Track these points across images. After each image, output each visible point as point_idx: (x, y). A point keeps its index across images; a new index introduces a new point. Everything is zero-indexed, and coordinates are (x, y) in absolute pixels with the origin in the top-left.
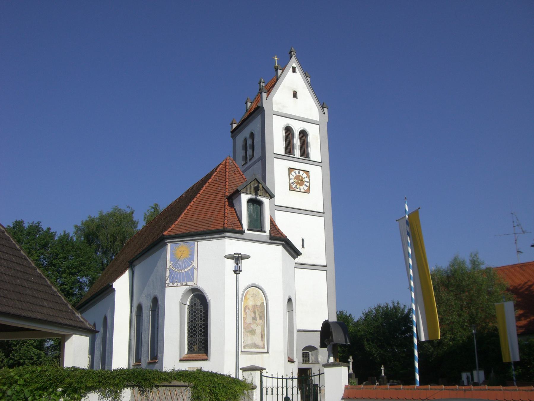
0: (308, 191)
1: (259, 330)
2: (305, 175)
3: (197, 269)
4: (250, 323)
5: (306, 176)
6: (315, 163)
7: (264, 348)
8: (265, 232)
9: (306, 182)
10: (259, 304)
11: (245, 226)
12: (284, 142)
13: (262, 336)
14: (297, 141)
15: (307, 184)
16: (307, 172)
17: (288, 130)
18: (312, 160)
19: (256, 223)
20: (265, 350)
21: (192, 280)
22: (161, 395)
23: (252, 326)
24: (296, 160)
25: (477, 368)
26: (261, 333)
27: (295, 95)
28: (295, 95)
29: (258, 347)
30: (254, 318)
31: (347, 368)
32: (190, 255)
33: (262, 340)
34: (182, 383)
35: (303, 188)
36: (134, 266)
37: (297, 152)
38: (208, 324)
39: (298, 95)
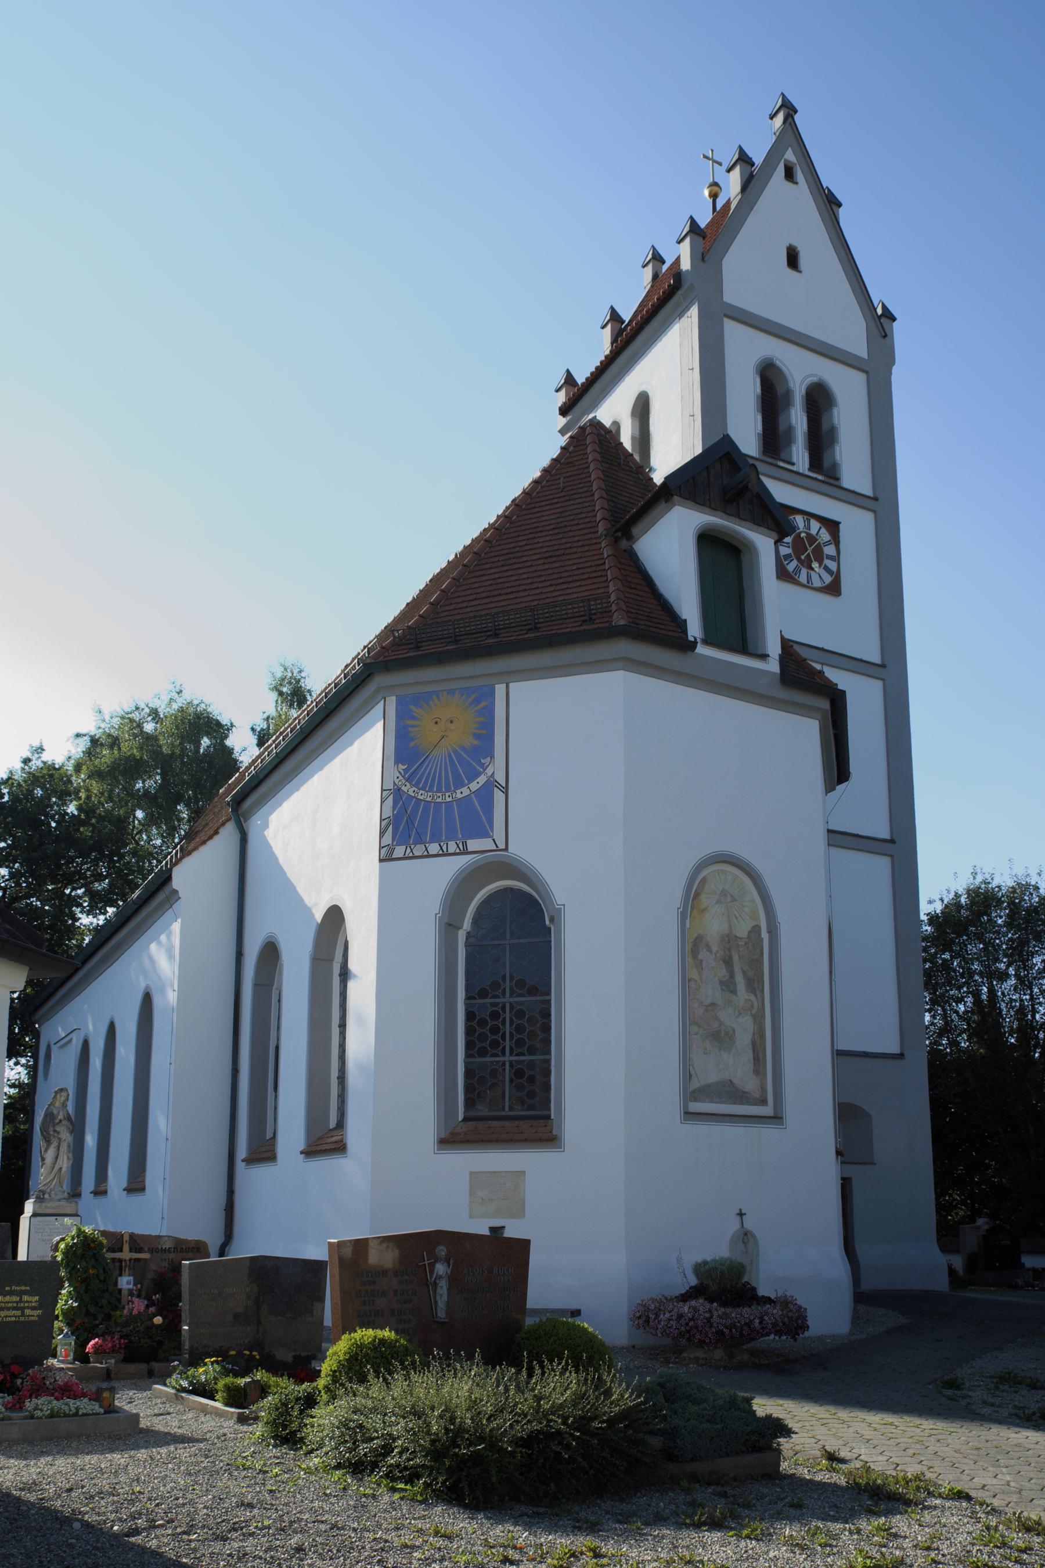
0: (834, 588)
1: (743, 1030)
2: (825, 536)
3: (506, 791)
6: (853, 498)
7: (763, 1102)
8: (764, 657)
9: (829, 557)
10: (742, 930)
12: (759, 418)
13: (758, 1059)
14: (798, 419)
15: (832, 565)
16: (832, 526)
19: (732, 617)
20: (768, 1110)
21: (484, 832)
22: (149, 1412)
23: (722, 1015)
26: (754, 1044)
27: (793, 259)
28: (793, 259)
29: (738, 1096)
30: (728, 985)
32: (476, 736)
35: (819, 576)
37: (800, 455)
39: (803, 260)
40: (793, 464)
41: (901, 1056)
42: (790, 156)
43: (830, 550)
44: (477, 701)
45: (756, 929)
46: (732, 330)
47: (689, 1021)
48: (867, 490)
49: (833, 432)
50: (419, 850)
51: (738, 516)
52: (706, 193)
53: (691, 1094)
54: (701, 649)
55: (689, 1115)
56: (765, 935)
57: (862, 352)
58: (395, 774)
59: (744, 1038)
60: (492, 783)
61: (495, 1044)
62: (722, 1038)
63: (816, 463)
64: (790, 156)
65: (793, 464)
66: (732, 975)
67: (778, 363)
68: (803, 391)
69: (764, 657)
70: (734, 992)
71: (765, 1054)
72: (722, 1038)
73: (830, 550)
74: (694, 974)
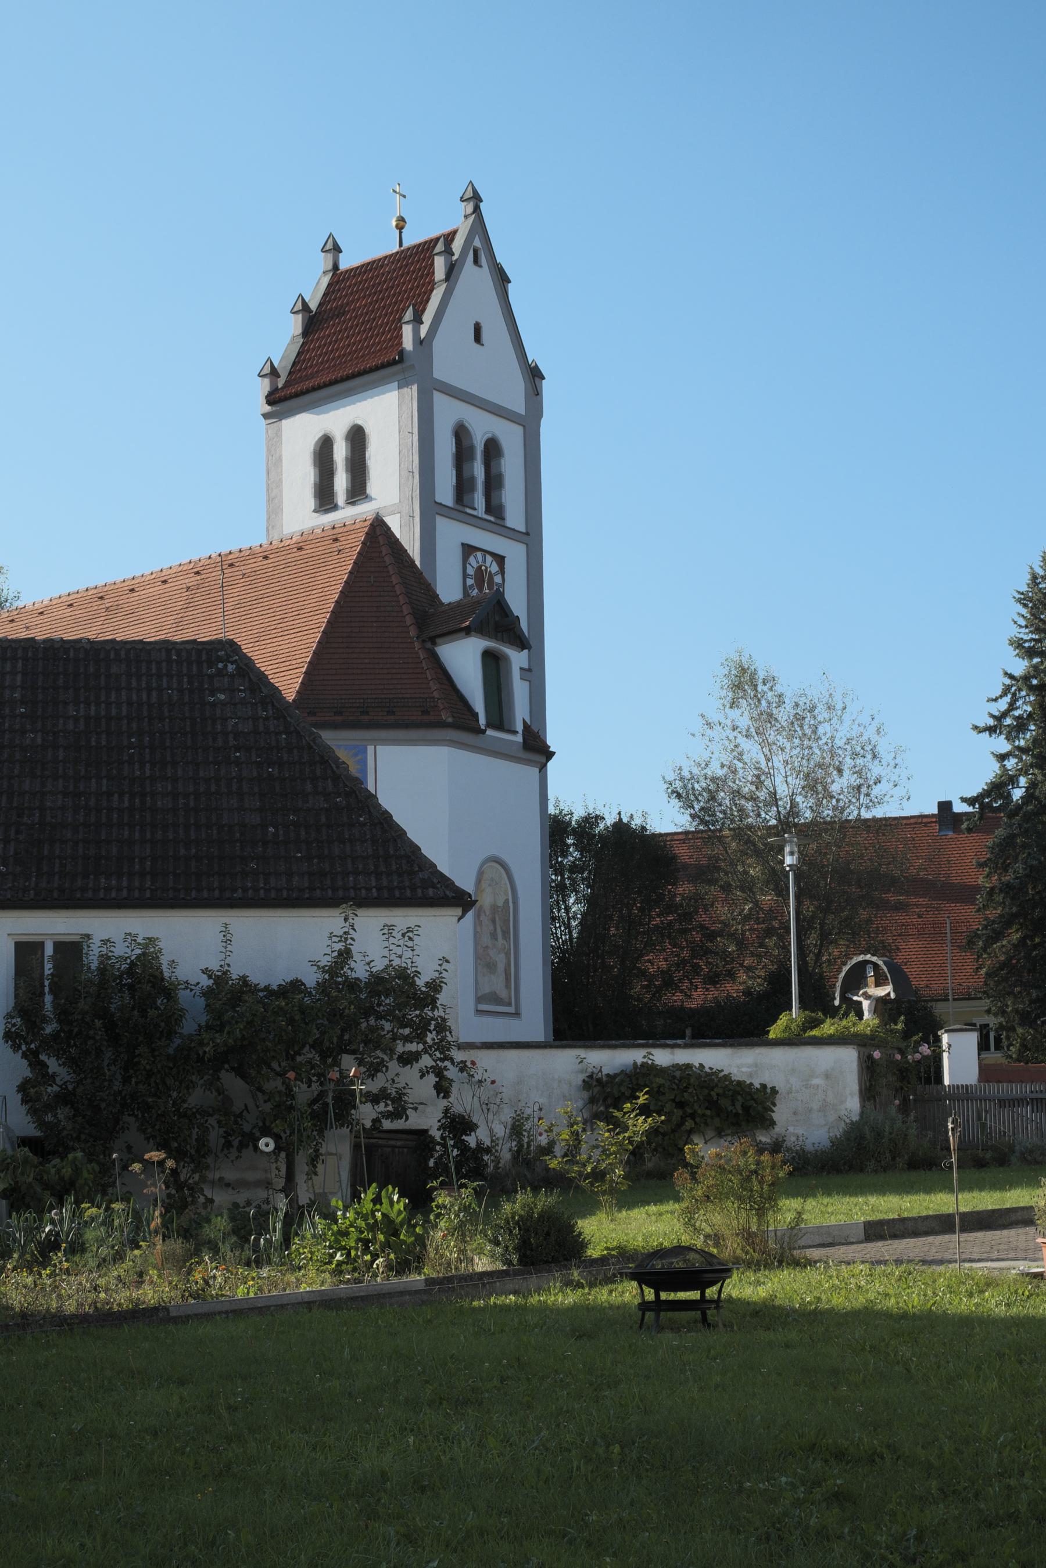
1: (500, 960)
2: (494, 568)
4: (487, 947)
6: (512, 534)
7: (509, 1004)
8: (515, 732)
10: (500, 903)
12: (454, 472)
16: (500, 560)
17: (461, 433)
20: (512, 1010)
24: (475, 522)
25: (49, 950)
30: (494, 936)
31: (541, 1038)
33: (508, 986)
37: (479, 500)
38: (66, 907)
40: (475, 509)
42: (477, 243)
44: (356, 755)
45: (507, 901)
46: (439, 398)
47: (477, 957)
48: (522, 528)
49: (500, 477)
51: (503, 641)
52: (394, 223)
53: (479, 1000)
54: (490, 732)
55: (479, 1012)
56: (511, 904)
57: (522, 411)
59: (501, 966)
62: (491, 967)
63: (489, 510)
64: (477, 243)
65: (475, 509)
66: (495, 929)
67: (467, 424)
69: (515, 732)
70: (496, 939)
71: (512, 978)
72: (491, 967)
74: (478, 929)
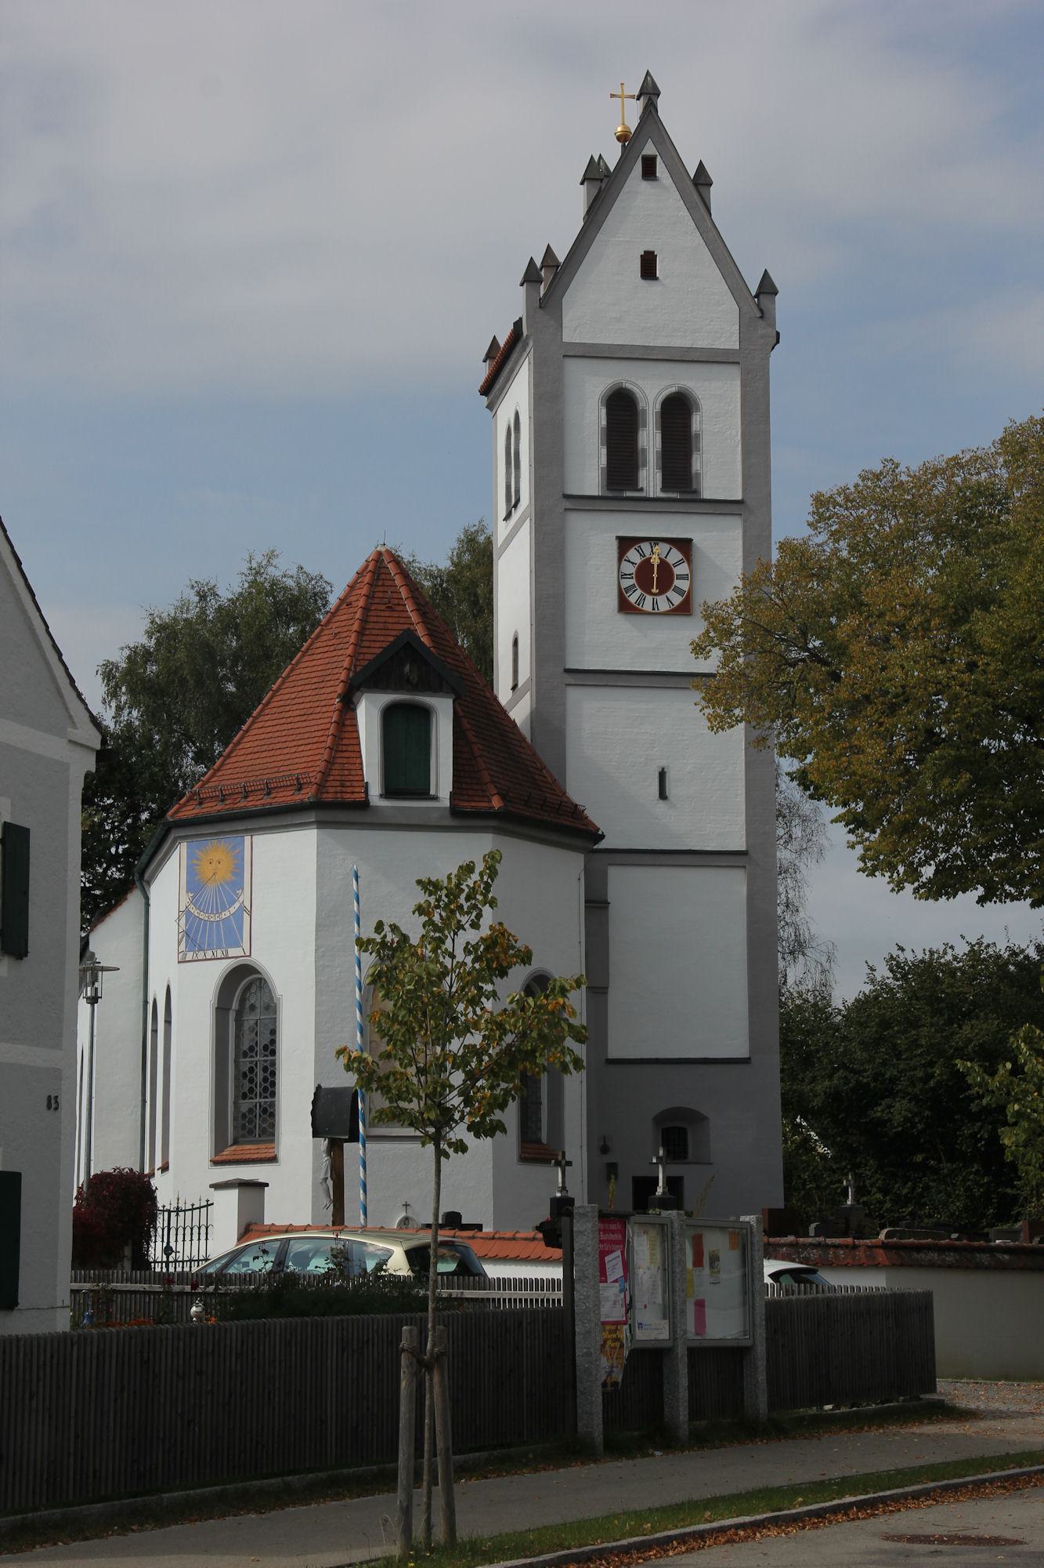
2: (675, 556)
5: (680, 556)
11: (375, 790)
14: (650, 439)
16: (684, 546)
17: (621, 407)
18: (706, 494)
21: (237, 944)
27: (648, 266)
28: (648, 266)
34: (411, 1131)
36: (149, 883)
37: (650, 479)
41: (745, 1061)
43: (682, 569)
50: (201, 955)
58: (185, 899)
60: (242, 908)
61: (251, 1090)
64: (650, 149)
65: (642, 490)
68: (658, 407)
69: (435, 798)
73: (682, 569)
